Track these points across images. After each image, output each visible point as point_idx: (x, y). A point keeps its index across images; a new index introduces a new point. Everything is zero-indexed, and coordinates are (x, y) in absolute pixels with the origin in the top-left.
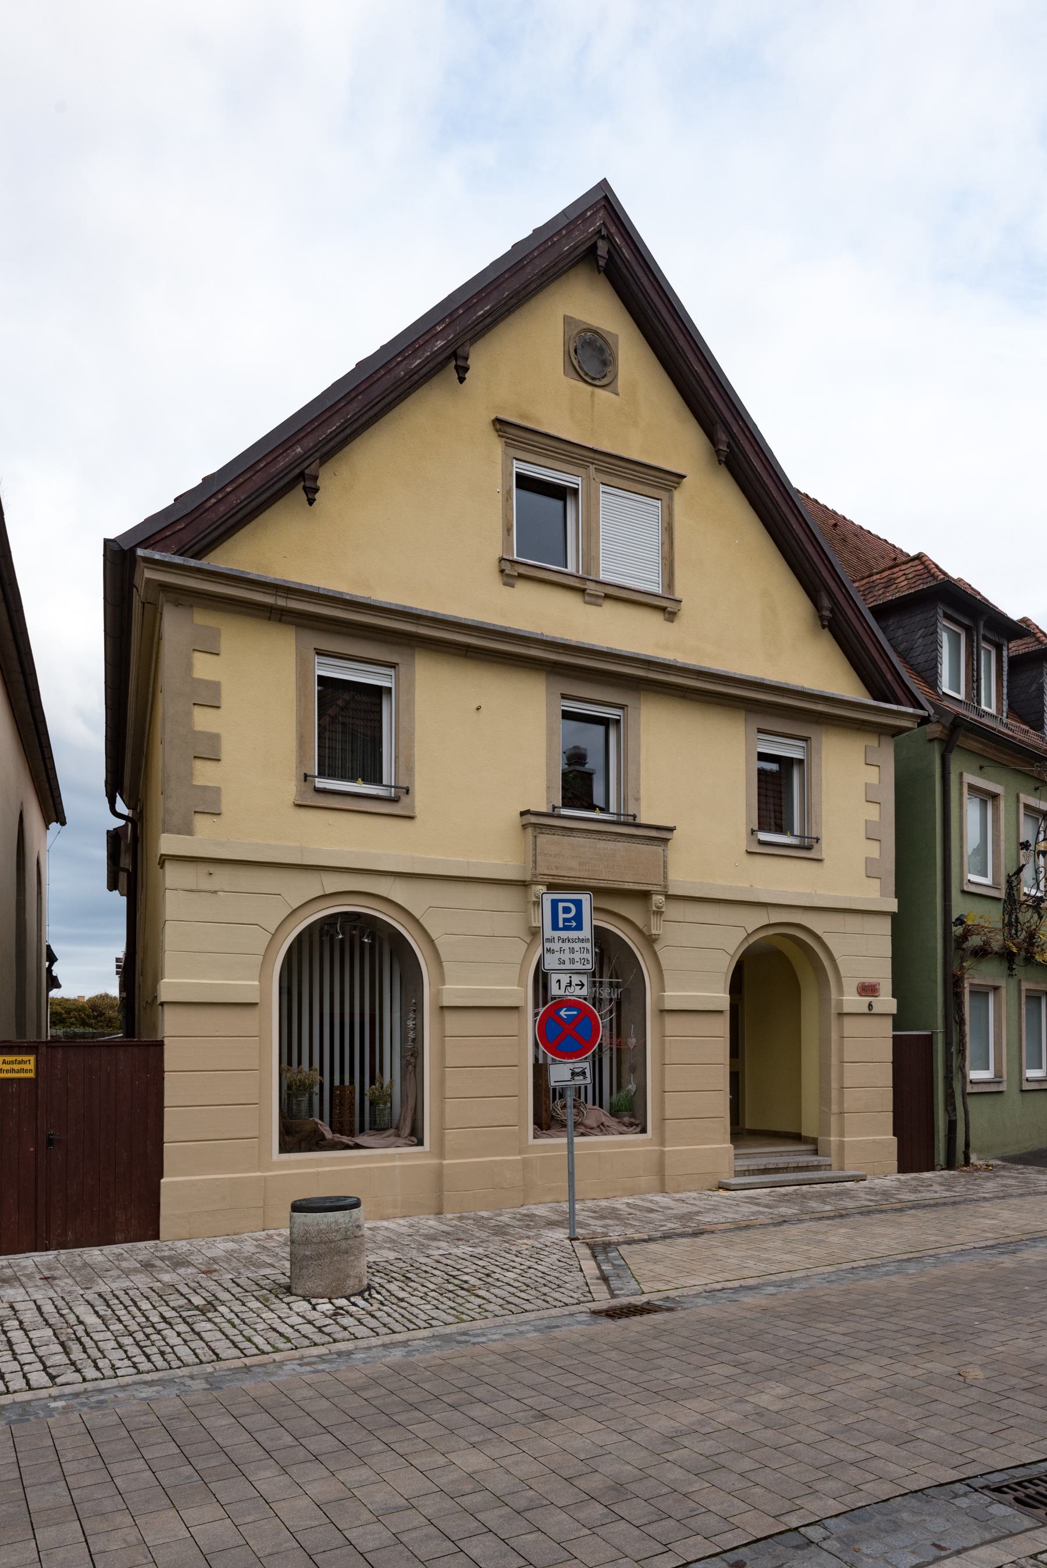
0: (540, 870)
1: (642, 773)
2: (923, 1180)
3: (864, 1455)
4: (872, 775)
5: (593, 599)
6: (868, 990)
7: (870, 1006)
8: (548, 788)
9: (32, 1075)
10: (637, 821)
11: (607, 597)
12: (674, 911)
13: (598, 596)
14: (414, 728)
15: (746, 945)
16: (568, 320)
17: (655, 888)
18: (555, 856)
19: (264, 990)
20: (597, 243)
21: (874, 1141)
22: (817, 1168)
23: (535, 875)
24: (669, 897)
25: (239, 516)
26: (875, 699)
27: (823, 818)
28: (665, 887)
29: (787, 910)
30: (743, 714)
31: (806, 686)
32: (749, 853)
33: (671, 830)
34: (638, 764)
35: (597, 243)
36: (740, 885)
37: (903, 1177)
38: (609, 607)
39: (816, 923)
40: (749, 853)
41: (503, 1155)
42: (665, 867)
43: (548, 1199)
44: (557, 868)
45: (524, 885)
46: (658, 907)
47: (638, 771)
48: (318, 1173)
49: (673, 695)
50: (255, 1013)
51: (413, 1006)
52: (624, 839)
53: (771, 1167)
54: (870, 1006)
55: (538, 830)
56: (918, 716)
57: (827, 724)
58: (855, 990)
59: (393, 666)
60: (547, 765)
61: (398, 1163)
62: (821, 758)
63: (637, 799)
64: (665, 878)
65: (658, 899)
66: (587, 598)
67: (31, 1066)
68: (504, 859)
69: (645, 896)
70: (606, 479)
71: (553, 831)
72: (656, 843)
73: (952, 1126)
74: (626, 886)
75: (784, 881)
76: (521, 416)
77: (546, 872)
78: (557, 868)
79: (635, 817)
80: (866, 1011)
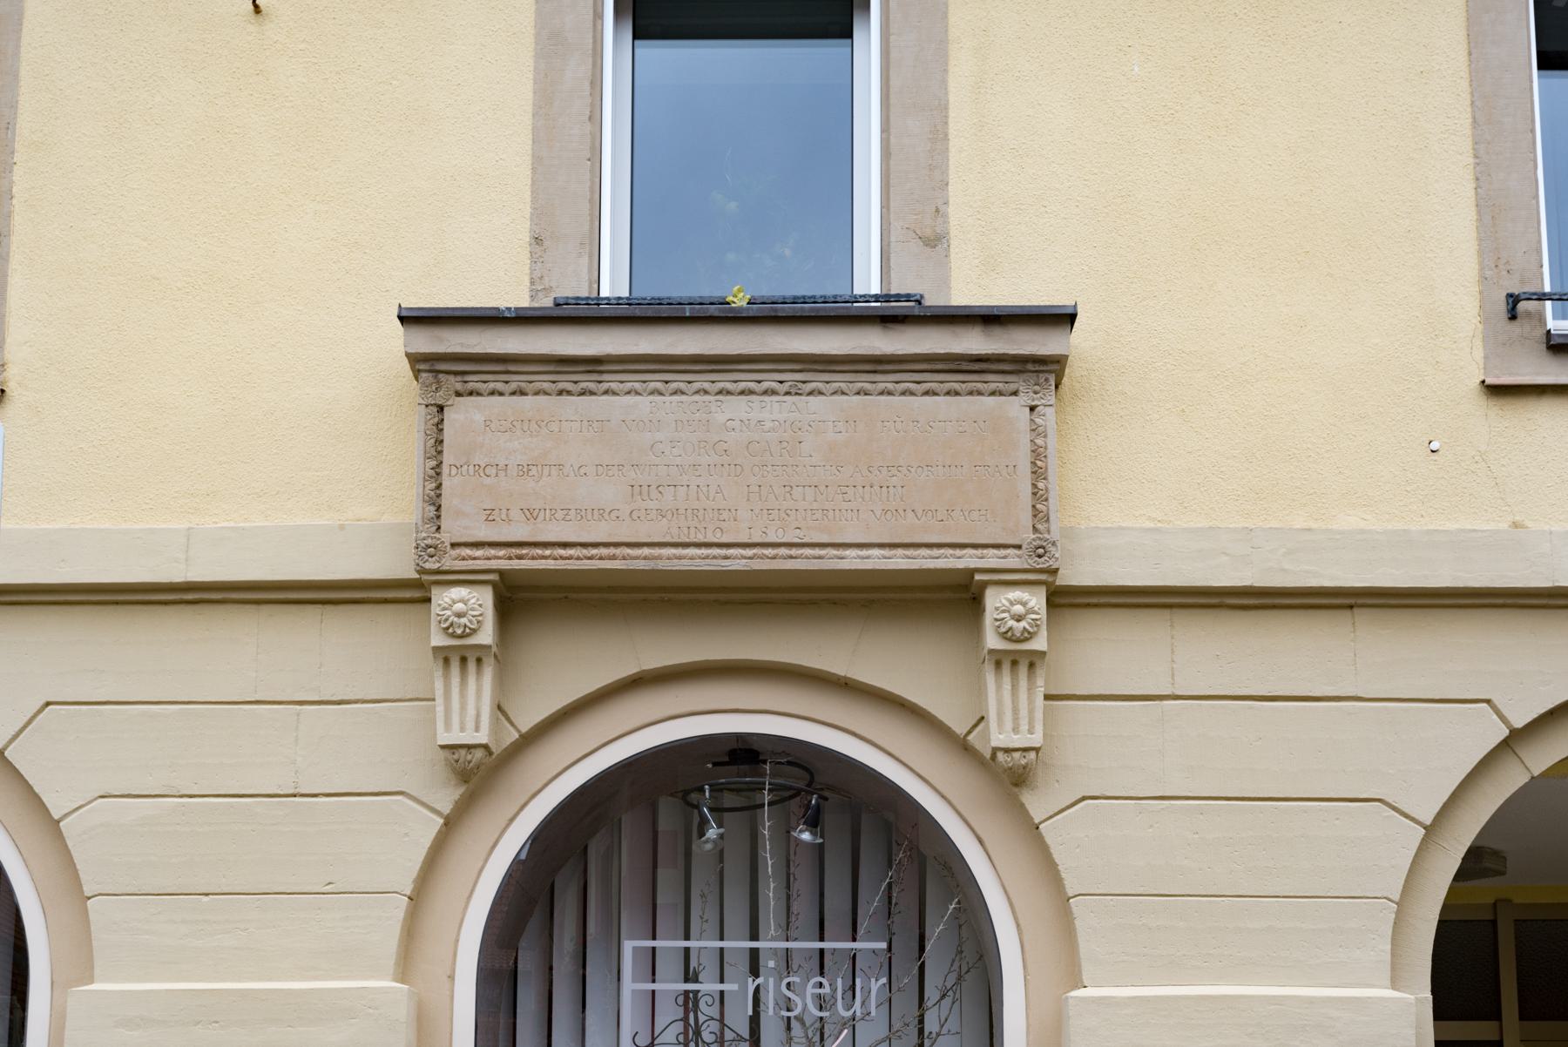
0: (454, 528)
1: (954, 144)
8: (537, 240)
12: (1111, 653)
14: (14, 106)
15: (1509, 781)
17: (992, 559)
18: (525, 470)
24: (1066, 600)
25: (1500, 601)
28: (1040, 551)
32: (1496, 391)
33: (1066, 318)
36: (1453, 526)
40: (1496, 391)
42: (1038, 473)
44: (530, 514)
45: (410, 594)
46: (1007, 635)
52: (839, 380)
55: (455, 383)
60: (537, 160)
64: (1039, 516)
65: (1010, 606)
68: (356, 517)
69: (953, 599)
71: (516, 382)
72: (995, 381)
78: (530, 514)
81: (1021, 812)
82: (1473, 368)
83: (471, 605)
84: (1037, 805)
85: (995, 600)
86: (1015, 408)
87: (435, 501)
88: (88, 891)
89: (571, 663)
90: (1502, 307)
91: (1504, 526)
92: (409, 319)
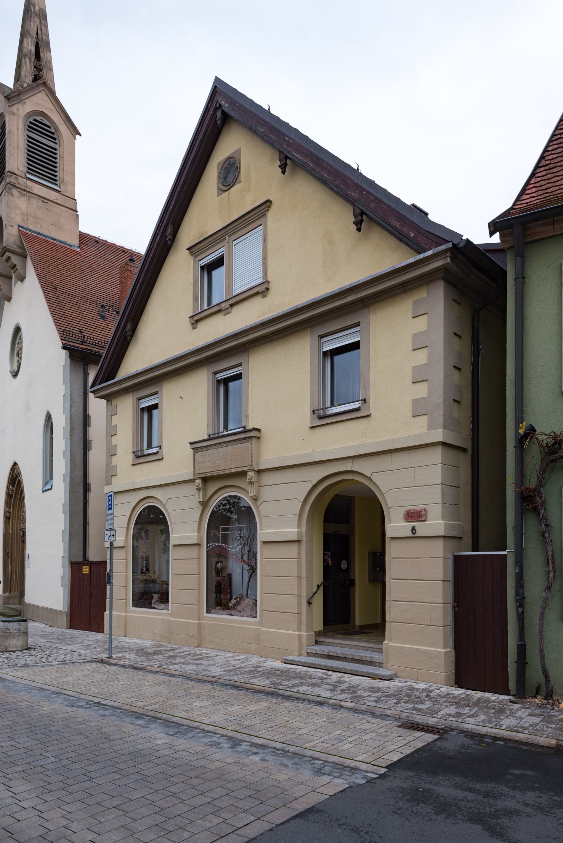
0: (197, 472)
2: (488, 700)
3: (28, 753)
4: (421, 324)
5: (226, 311)
6: (414, 516)
7: (413, 529)
9: (88, 573)
10: (247, 428)
11: (232, 306)
12: (267, 479)
13: (227, 308)
16: (238, 151)
19: (200, 537)
20: (225, 112)
21: (418, 651)
22: (371, 663)
23: (194, 475)
24: (259, 472)
26: (420, 253)
27: (371, 381)
28: (252, 466)
29: (339, 462)
30: (309, 331)
31: (248, 324)
32: (312, 428)
34: (247, 394)
35: (225, 112)
37: (459, 692)
38: (235, 309)
39: (357, 466)
41: (192, 620)
43: (211, 646)
44: (203, 469)
47: (247, 399)
48: (139, 617)
49: (266, 343)
50: (124, 550)
51: (250, 540)
52: (232, 443)
53: (332, 654)
54: (413, 529)
56: (445, 251)
57: (372, 304)
58: (402, 517)
59: (358, 324)
61: (161, 617)
62: (248, 373)
63: (247, 416)
66: (224, 313)
67: (88, 570)
68: (187, 472)
69: (243, 474)
70: (234, 237)
72: (247, 440)
73: (522, 650)
74: (233, 471)
75: (149, 474)
76: (200, 237)
77: (199, 472)
79: (244, 427)
80: (410, 534)
81: (256, 504)
82: (131, 462)
83: (198, 482)
84: (258, 503)
85: (249, 474)
86: (249, 444)
87: (194, 468)
88: (389, 506)
89: (212, 487)
90: (367, 400)
91: (311, 451)
92: (191, 444)
